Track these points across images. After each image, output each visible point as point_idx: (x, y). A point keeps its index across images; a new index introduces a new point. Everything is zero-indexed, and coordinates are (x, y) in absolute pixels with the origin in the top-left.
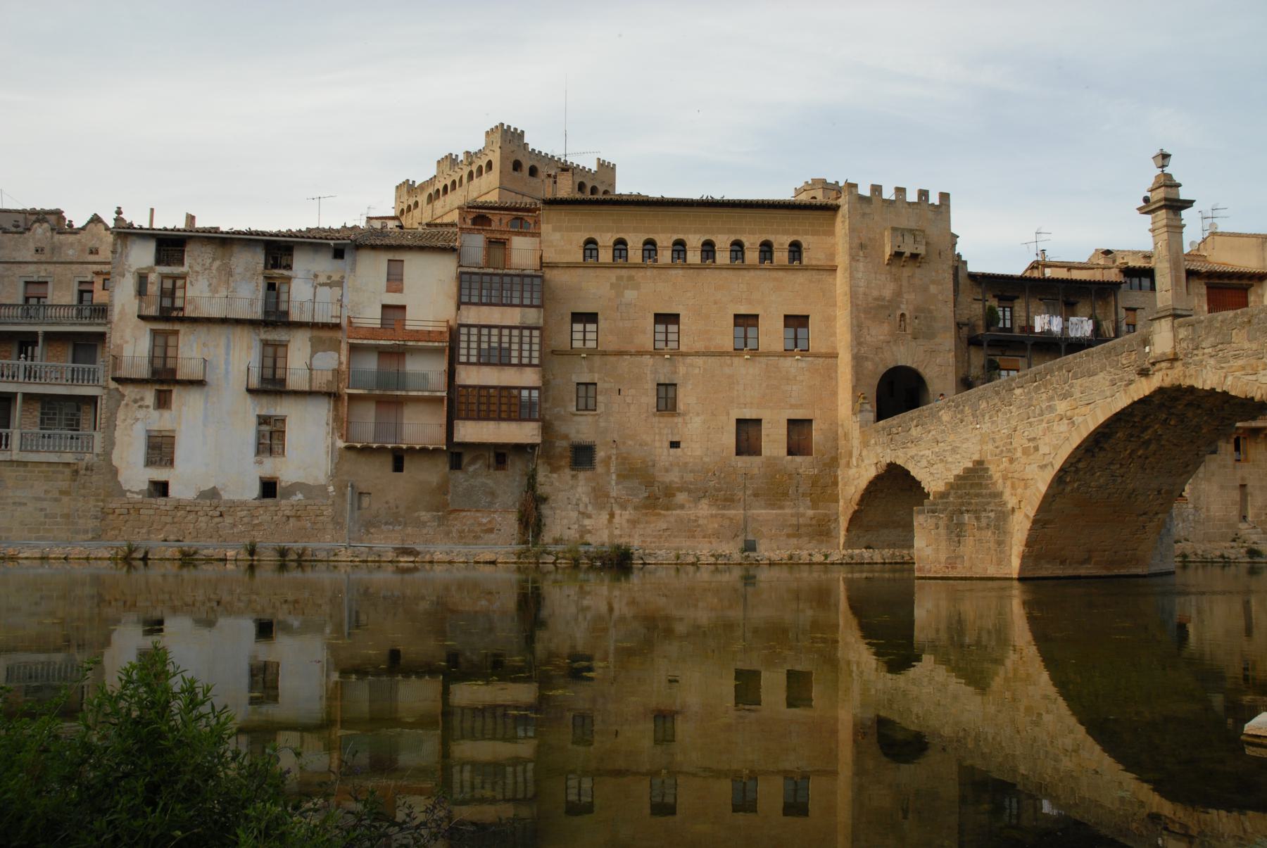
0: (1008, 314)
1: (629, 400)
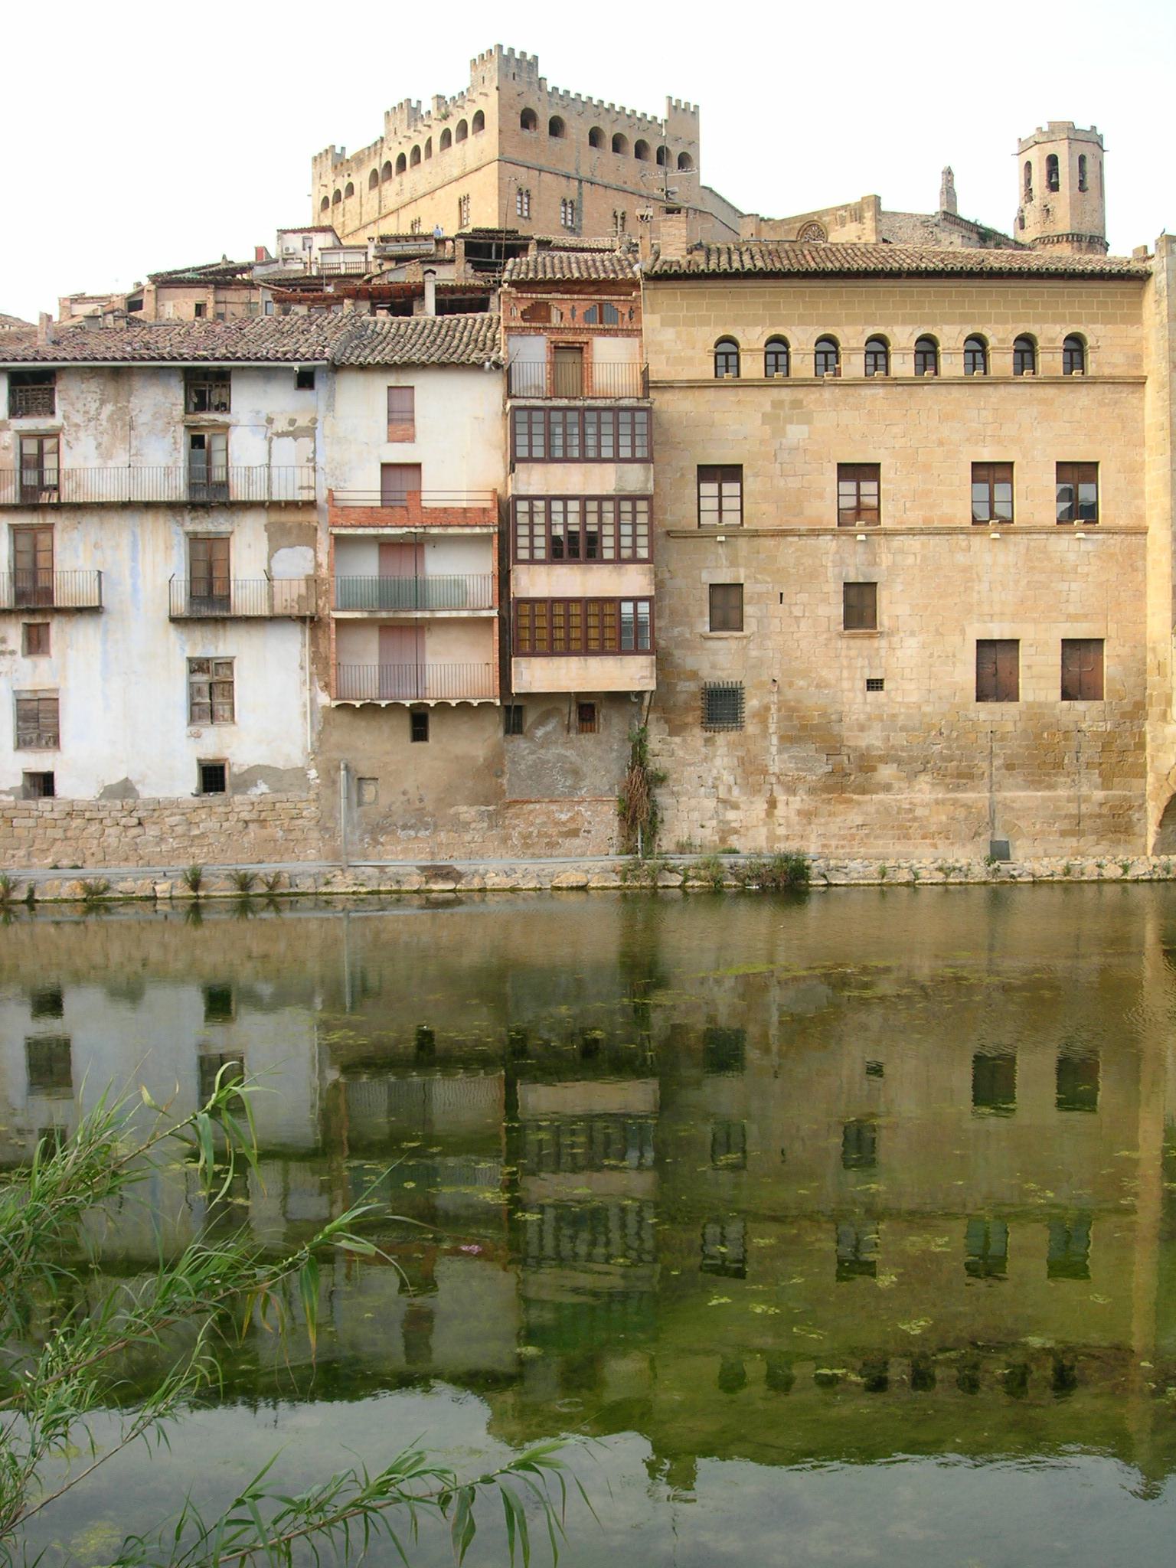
1: (797, 611)
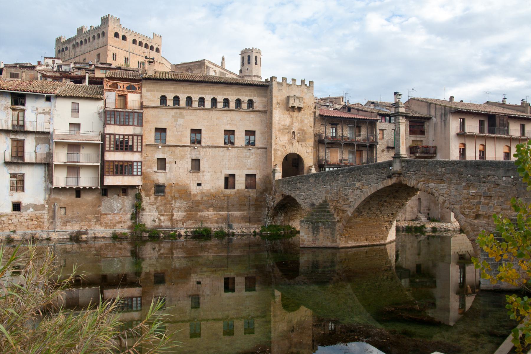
0: (334, 131)
1: (179, 166)
